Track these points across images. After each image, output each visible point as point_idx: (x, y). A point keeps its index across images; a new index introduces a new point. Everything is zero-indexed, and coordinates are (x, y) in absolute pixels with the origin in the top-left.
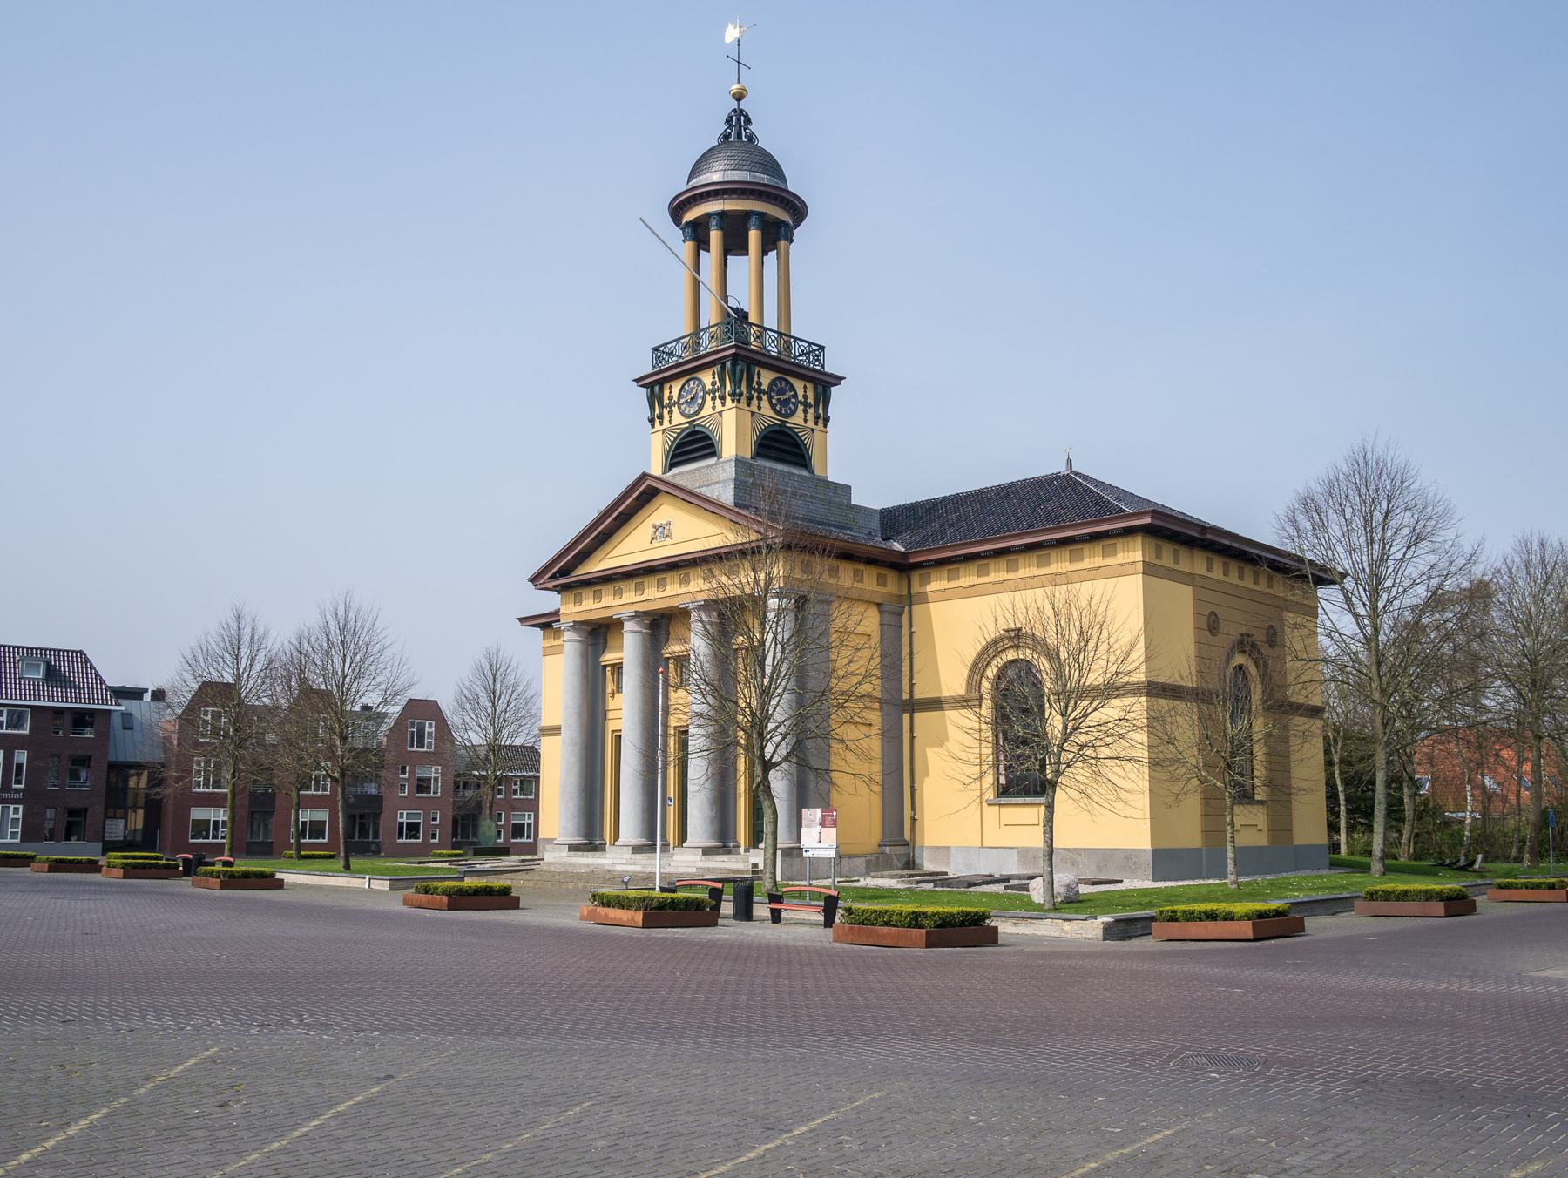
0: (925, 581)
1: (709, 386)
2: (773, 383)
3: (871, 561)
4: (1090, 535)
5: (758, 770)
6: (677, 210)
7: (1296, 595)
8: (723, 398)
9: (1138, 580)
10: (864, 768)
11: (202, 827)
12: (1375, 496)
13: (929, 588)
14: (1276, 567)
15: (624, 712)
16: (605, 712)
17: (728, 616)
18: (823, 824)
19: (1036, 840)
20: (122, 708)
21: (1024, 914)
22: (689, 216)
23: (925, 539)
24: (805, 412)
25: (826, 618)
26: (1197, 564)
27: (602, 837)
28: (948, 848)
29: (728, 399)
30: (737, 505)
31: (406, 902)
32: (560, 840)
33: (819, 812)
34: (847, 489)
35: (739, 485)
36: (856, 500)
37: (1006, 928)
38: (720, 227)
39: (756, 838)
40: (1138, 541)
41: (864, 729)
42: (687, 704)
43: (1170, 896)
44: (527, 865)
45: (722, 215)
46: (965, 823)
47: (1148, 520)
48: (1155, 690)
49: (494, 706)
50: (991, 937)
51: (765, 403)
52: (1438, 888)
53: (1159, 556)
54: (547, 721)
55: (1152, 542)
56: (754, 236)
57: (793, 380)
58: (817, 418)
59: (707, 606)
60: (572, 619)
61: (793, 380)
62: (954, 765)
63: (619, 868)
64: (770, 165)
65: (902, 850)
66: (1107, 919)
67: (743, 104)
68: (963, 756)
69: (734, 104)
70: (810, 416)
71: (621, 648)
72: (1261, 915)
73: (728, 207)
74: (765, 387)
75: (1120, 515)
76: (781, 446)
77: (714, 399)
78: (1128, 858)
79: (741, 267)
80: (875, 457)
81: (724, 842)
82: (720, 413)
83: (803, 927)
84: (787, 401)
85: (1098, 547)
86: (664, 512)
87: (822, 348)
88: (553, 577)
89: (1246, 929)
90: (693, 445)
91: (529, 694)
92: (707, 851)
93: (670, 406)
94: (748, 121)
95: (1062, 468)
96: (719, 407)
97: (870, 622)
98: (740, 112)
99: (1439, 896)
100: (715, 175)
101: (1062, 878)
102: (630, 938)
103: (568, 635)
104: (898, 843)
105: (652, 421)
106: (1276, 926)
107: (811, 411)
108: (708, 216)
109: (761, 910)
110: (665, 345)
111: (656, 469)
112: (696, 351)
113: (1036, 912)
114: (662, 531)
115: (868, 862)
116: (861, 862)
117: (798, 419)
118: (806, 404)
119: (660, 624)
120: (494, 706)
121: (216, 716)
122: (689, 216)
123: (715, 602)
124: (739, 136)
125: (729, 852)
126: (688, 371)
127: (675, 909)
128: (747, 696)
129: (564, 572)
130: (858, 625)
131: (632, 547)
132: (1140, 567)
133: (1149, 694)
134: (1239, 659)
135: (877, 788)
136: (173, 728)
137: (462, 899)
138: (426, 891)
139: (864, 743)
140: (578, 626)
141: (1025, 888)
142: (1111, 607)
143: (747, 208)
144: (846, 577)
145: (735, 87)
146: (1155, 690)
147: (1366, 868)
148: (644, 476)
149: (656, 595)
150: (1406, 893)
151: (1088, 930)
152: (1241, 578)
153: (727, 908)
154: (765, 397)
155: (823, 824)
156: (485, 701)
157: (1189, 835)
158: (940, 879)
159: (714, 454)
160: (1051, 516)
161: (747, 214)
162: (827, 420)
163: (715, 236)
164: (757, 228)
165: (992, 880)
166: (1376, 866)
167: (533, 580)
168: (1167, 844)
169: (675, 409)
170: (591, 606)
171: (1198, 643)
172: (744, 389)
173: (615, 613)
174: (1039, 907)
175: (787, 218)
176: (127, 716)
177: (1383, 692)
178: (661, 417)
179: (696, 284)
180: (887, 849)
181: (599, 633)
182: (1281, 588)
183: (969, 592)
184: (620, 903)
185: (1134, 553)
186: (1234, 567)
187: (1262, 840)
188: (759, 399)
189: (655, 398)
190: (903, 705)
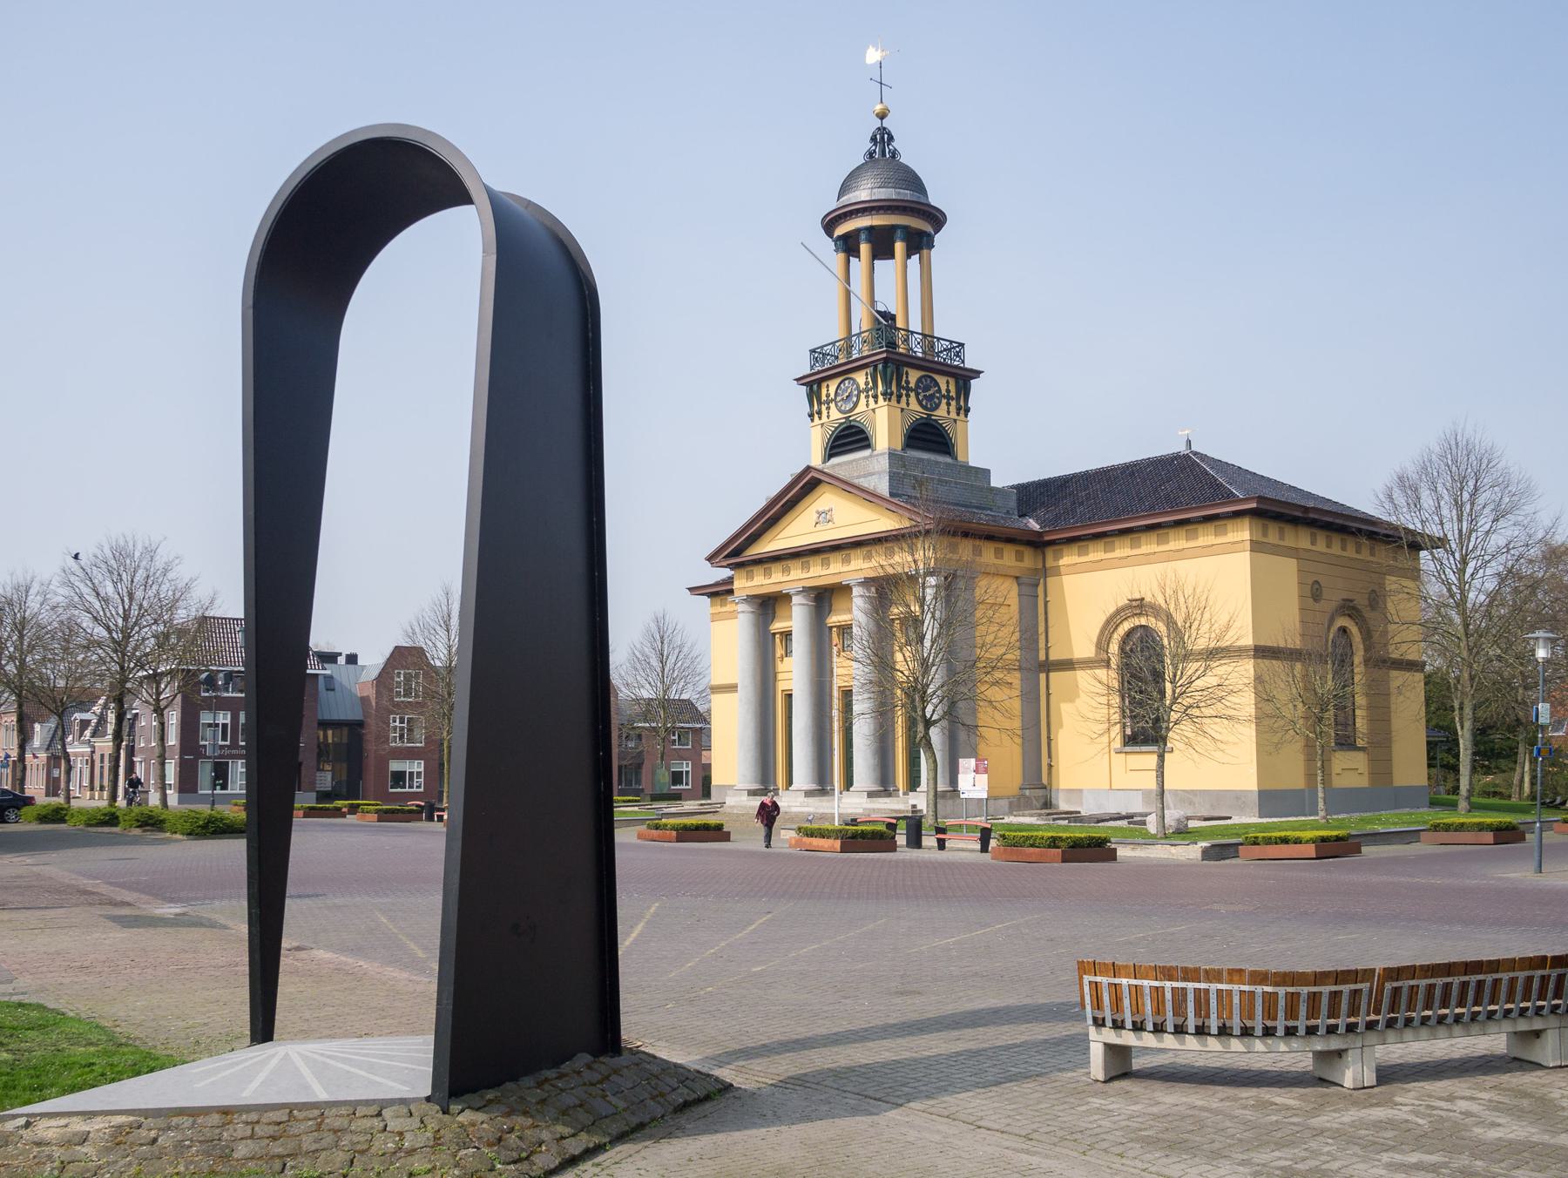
0: (1057, 557)
1: (862, 386)
2: (919, 380)
3: (1010, 540)
5: (921, 728)
6: (829, 225)
7: (1404, 560)
8: (875, 397)
9: (1245, 557)
10: (1007, 724)
11: (399, 778)
12: (1465, 474)
13: (1061, 562)
14: (1372, 536)
15: (794, 673)
16: (775, 674)
17: (884, 589)
18: (976, 771)
19: (1152, 784)
20: (328, 672)
21: (1140, 840)
22: (841, 230)
23: (1057, 517)
24: (948, 404)
25: (971, 588)
26: (1301, 539)
27: (775, 783)
28: (1081, 791)
29: (881, 398)
30: (892, 494)
31: (640, 836)
33: (973, 761)
34: (986, 472)
35: (893, 477)
36: (997, 481)
37: (1123, 852)
38: (868, 241)
39: (913, 783)
40: (1246, 522)
41: (1007, 691)
42: (849, 670)
43: (1265, 828)
44: (707, 808)
45: (871, 229)
46: (1093, 767)
47: (1254, 505)
48: (1262, 652)
49: (663, 663)
50: (1111, 856)
52: (1488, 820)
53: (1265, 535)
54: (717, 680)
55: (1259, 522)
56: (899, 247)
57: (936, 377)
58: (959, 409)
59: (867, 582)
60: (744, 594)
61: (936, 377)
62: (1085, 713)
63: (794, 810)
64: (913, 181)
65: (1040, 792)
66: (1205, 844)
67: (886, 123)
68: (1090, 715)
70: (953, 408)
71: (790, 618)
72: (1324, 840)
74: (912, 385)
75: (1229, 498)
76: (928, 437)
78: (1237, 797)
79: (886, 270)
80: (1007, 443)
81: (885, 787)
83: (964, 847)
84: (932, 396)
85: (1210, 527)
86: (825, 499)
87: (962, 345)
89: (1311, 850)
90: (849, 438)
91: (694, 654)
92: (871, 795)
94: (891, 138)
95: (1181, 448)
96: (872, 404)
97: (1009, 593)
98: (882, 130)
99: (1490, 828)
100: (863, 194)
101: (1173, 815)
102: (832, 859)
103: (743, 607)
104: (1036, 786)
105: (811, 415)
106: (1334, 848)
107: (953, 403)
108: (858, 231)
109: (929, 841)
111: (816, 460)
112: (849, 353)
113: (1150, 840)
114: (825, 516)
115: (1011, 804)
116: (1004, 803)
117: (941, 412)
118: (949, 398)
119: (824, 598)
120: (663, 663)
121: (408, 678)
122: (841, 230)
123: (873, 579)
124: (884, 154)
125: (890, 795)
126: (845, 372)
127: (863, 839)
128: (903, 661)
129: (737, 552)
130: (997, 594)
131: (798, 531)
132: (1248, 545)
133: (1255, 657)
134: (1342, 622)
135: (1019, 741)
137: (689, 833)
138: (657, 827)
139: (1007, 704)
140: (751, 599)
141: (1144, 823)
142: (1216, 584)
143: (894, 219)
144: (987, 554)
145: (878, 107)
146: (1262, 652)
147: (1453, 806)
148: (808, 469)
150: (1462, 825)
151: (1191, 852)
152: (1344, 549)
153: (901, 840)
155: (976, 771)
156: (655, 662)
157: (1293, 776)
158: (1074, 817)
159: (868, 446)
160: (1168, 495)
161: (893, 228)
162: (967, 410)
163: (864, 248)
165: (1121, 818)
166: (1463, 805)
167: (710, 559)
168: (1267, 787)
169: (832, 405)
171: (1302, 609)
172: (894, 388)
173: (785, 589)
174: (1153, 837)
175: (930, 229)
176: (329, 678)
177: (1470, 650)
178: (819, 413)
179: (848, 294)
180: (1027, 792)
181: (768, 605)
182: (1382, 556)
183: (1098, 566)
184: (822, 834)
185: (1242, 533)
186: (1337, 540)
187: (1362, 782)
188: (908, 396)
190: (1039, 667)
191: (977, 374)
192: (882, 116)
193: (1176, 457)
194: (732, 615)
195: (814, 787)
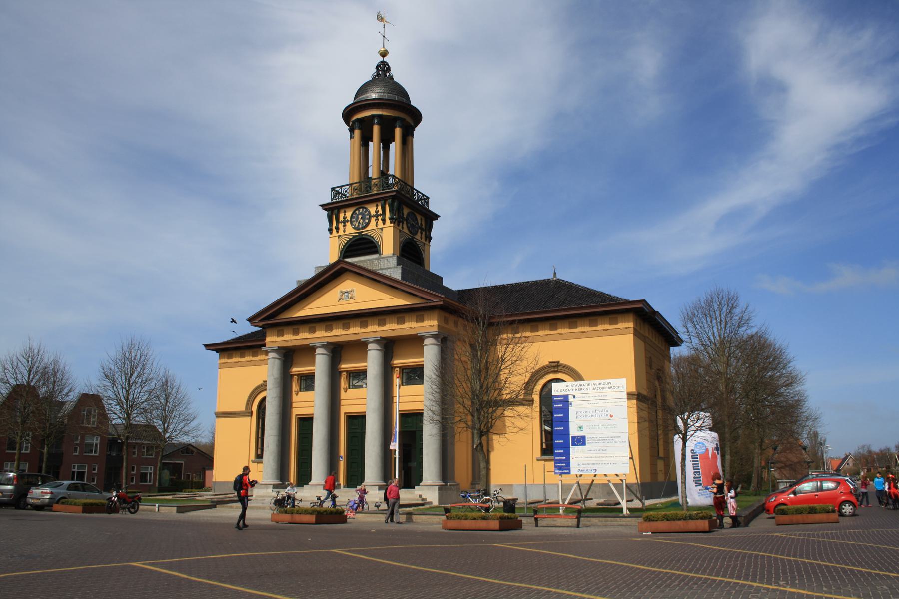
4: (521, 320)
8: (384, 220)
16: (291, 403)
28: (511, 485)
29: (388, 221)
32: (266, 481)
38: (378, 124)
45: (380, 117)
51: (405, 226)
60: (276, 346)
69: (381, 59)
73: (385, 113)
76: (412, 253)
77: (377, 220)
82: (382, 229)
88: (260, 321)
94: (389, 69)
95: (550, 276)
98: (384, 63)
105: (330, 230)
108: (373, 117)
117: (418, 237)
119: (337, 351)
132: (632, 331)
136: (73, 396)
149: (339, 334)
163: (376, 129)
164: (400, 127)
169: (348, 224)
170: (289, 339)
178: (337, 229)
181: (288, 356)
191: (436, 217)
192: (384, 54)
193: (547, 282)
194: (264, 363)
195: (277, 482)
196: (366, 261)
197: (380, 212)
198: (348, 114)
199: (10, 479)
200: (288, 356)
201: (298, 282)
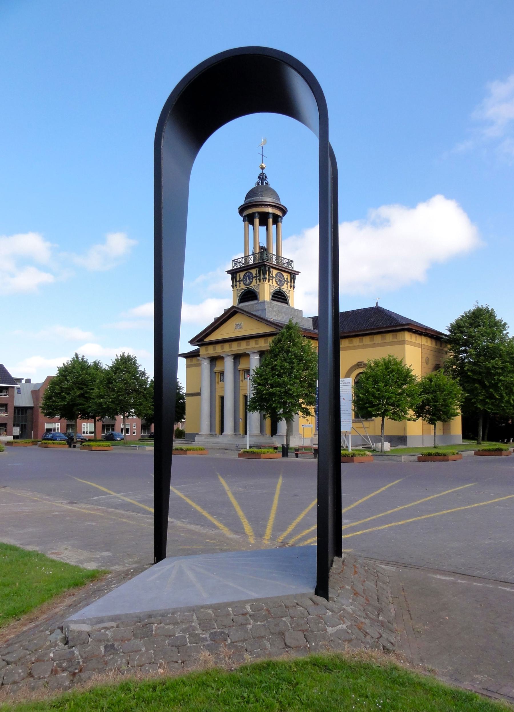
1: (254, 275)
2: (277, 274)
8: (260, 280)
24: (287, 284)
51: (274, 281)
58: (291, 286)
69: (261, 171)
74: (274, 276)
77: (256, 279)
87: (292, 261)
93: (240, 281)
96: (258, 283)
105: (232, 286)
107: (289, 284)
110: (237, 259)
149: (236, 348)
154: (274, 279)
162: (294, 287)
178: (236, 285)
188: (272, 280)
189: (234, 278)
196: (246, 306)
197: (258, 275)
198: (241, 210)
199: (491, 382)
200: (214, 360)
201: (214, 318)
